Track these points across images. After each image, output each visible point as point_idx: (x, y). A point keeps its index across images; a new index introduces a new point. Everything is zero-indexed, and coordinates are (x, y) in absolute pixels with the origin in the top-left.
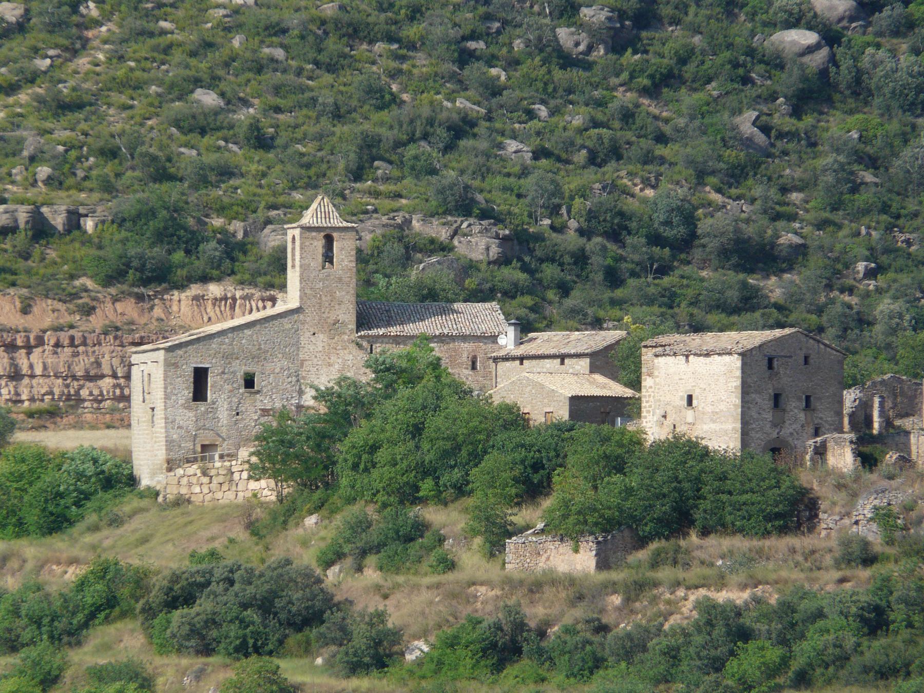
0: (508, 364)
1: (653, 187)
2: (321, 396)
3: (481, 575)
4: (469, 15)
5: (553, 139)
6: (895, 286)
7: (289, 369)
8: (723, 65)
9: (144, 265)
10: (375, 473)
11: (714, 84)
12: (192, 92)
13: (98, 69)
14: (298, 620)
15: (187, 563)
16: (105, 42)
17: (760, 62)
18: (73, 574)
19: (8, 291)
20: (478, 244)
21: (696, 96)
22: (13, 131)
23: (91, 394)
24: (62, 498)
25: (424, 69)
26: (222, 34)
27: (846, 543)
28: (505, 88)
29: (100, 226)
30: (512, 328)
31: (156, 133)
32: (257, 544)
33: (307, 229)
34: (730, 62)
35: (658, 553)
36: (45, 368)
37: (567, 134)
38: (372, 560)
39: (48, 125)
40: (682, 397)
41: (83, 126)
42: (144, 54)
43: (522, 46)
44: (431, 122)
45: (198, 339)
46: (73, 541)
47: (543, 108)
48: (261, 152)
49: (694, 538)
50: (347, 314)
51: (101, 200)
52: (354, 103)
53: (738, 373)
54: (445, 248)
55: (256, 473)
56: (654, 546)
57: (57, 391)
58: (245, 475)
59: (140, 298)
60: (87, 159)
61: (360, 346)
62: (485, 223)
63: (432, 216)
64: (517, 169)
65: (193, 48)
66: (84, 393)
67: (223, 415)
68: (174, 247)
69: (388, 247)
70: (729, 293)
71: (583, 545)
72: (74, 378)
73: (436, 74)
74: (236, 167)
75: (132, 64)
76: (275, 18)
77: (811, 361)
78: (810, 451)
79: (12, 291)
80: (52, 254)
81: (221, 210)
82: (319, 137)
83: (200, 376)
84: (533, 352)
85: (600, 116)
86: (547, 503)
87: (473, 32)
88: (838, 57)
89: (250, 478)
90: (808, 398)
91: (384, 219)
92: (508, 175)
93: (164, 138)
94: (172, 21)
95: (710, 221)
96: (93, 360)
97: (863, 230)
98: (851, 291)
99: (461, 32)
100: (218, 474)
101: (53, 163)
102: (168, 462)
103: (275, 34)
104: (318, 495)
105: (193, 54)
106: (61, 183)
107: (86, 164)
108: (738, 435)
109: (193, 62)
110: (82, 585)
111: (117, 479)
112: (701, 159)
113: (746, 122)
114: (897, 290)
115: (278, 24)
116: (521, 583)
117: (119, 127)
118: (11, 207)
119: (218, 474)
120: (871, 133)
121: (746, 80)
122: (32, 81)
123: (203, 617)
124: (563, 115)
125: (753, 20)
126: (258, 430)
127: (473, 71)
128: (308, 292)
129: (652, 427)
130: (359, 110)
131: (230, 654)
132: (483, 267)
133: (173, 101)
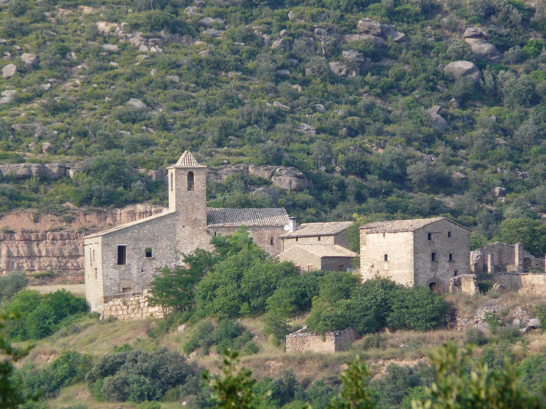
0: (290, 241)
1: (383, 148)
2: (188, 260)
3: (273, 355)
4: (281, 56)
5: (327, 123)
6: (516, 199)
7: (170, 246)
8: (421, 81)
9: (101, 195)
10: (215, 300)
11: (416, 91)
12: (128, 100)
13: (76, 89)
14: (173, 380)
15: (113, 352)
16: (80, 74)
17: (441, 79)
18: (52, 359)
19: (26, 210)
20: (285, 180)
21: (407, 98)
22: (29, 123)
23: (73, 265)
24: (47, 319)
25: (257, 86)
26: (144, 68)
27: (470, 333)
28: (301, 95)
29: (77, 174)
30: (292, 221)
31: (109, 125)
32: (152, 341)
33: (178, 169)
34: (425, 79)
35: (368, 341)
36: (47, 251)
37: (335, 120)
38: (213, 348)
39: (49, 119)
40: (382, 256)
41: (68, 120)
42: (101, 80)
43: (310, 72)
44: (260, 114)
45: (120, 230)
46: (53, 342)
47: (322, 106)
48: (166, 132)
49: (388, 332)
50: (201, 216)
51: (78, 160)
52: (218, 105)
53: (412, 242)
54: (267, 183)
55: (152, 302)
56: (366, 337)
57: (54, 264)
58: (147, 303)
59: (99, 212)
60: (70, 138)
61: (208, 232)
62: (289, 168)
63: (260, 165)
64: (307, 139)
65: (128, 76)
66: (69, 265)
67: (135, 272)
68: (121, 186)
69: (235, 182)
70: (424, 205)
71: (328, 337)
72: (64, 257)
73: (262, 89)
74: (152, 141)
75: (95, 85)
76: (174, 59)
77: (452, 235)
78: (452, 283)
79: (29, 210)
80: (51, 190)
81: (144, 164)
82: (198, 124)
83: (121, 250)
84: (303, 234)
85: (353, 110)
86: (309, 316)
87: (283, 65)
88: (484, 75)
89: (149, 305)
90: (450, 255)
91: (233, 168)
92: (302, 142)
93: (113, 125)
94: (117, 62)
95: (413, 166)
96: (73, 247)
97: (499, 170)
98: (491, 202)
99: (277, 65)
100: (132, 304)
101: (52, 140)
102: (105, 298)
103: (174, 68)
104: (184, 314)
105: (129, 79)
106: (55, 152)
107: (70, 141)
108: (412, 276)
109: (129, 84)
110: (55, 366)
111: (80, 306)
112: (409, 132)
113: (434, 111)
114: (517, 202)
115: (175, 63)
116: (294, 358)
117: (88, 120)
118: (27, 164)
119: (132, 304)
120: (503, 117)
121: (433, 89)
122: (40, 96)
123: (121, 381)
124: (333, 109)
125: (437, 56)
126: (153, 279)
127: (284, 86)
128: (180, 203)
129: (366, 273)
130: (220, 109)
131: (135, 400)
132: (288, 192)
133: (117, 105)
